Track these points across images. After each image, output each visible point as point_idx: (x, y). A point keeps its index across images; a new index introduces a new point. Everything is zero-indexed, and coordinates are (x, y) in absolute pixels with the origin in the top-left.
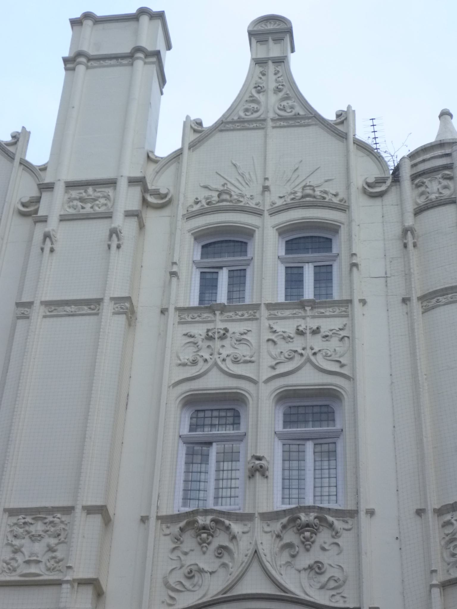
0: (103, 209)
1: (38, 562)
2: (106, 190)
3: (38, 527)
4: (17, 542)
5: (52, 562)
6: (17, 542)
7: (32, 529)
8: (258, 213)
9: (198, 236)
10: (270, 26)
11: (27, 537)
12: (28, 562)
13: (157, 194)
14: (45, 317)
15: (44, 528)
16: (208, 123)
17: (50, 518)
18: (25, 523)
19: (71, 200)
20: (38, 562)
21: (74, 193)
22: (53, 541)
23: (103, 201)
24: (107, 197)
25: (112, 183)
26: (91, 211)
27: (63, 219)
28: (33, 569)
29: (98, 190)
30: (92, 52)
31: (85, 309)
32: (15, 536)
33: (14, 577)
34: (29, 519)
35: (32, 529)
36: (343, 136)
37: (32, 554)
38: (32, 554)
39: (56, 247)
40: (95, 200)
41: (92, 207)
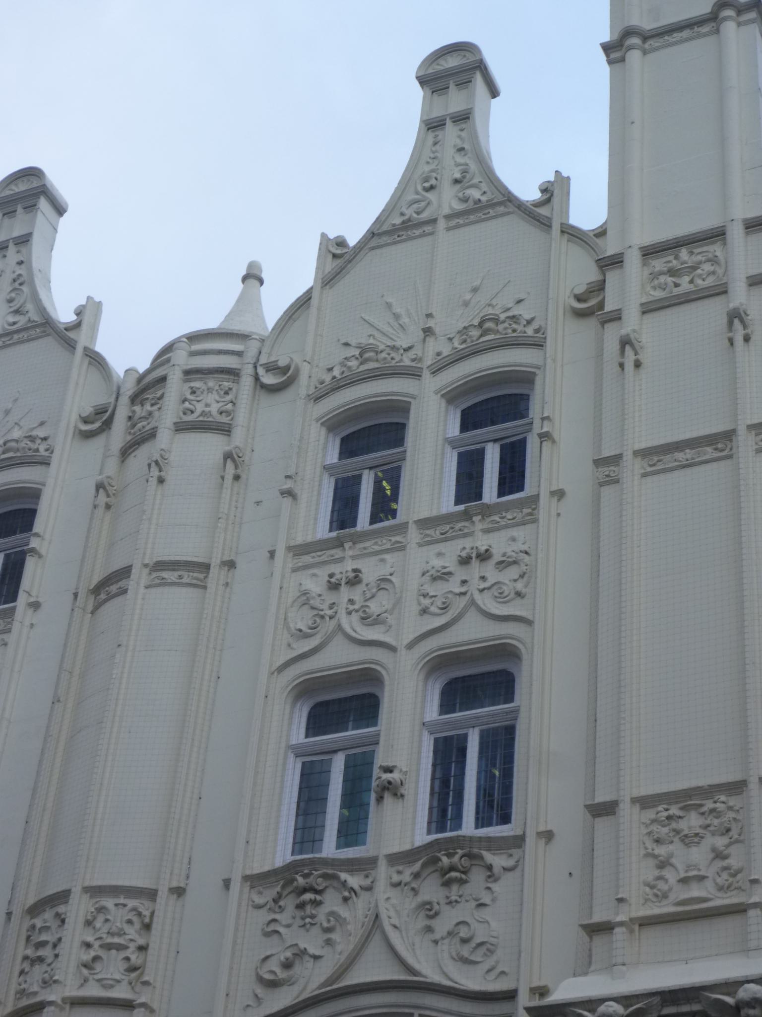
0: (710, 281)
1: (701, 878)
2: (710, 248)
3: (692, 822)
4: (661, 851)
5: (725, 875)
6: (661, 851)
7: (682, 825)
8: (414, 374)
9: (332, 425)
10: (452, 62)
11: (676, 839)
12: (684, 881)
13: (272, 368)
14: (644, 475)
15: (702, 821)
16: (352, 241)
17: (709, 805)
18: (669, 818)
19: (654, 276)
20: (701, 878)
21: (658, 264)
22: (720, 842)
23: (707, 267)
24: (714, 261)
25: (718, 235)
26: (692, 287)
27: (648, 309)
28: (695, 891)
29: (696, 251)
30: (648, 25)
31: (709, 452)
32: (657, 841)
33: (667, 908)
34: (674, 810)
35: (682, 825)
36: (71, 345)
37: (689, 868)
38: (689, 868)
39: (643, 357)
40: (694, 268)
41: (691, 282)
